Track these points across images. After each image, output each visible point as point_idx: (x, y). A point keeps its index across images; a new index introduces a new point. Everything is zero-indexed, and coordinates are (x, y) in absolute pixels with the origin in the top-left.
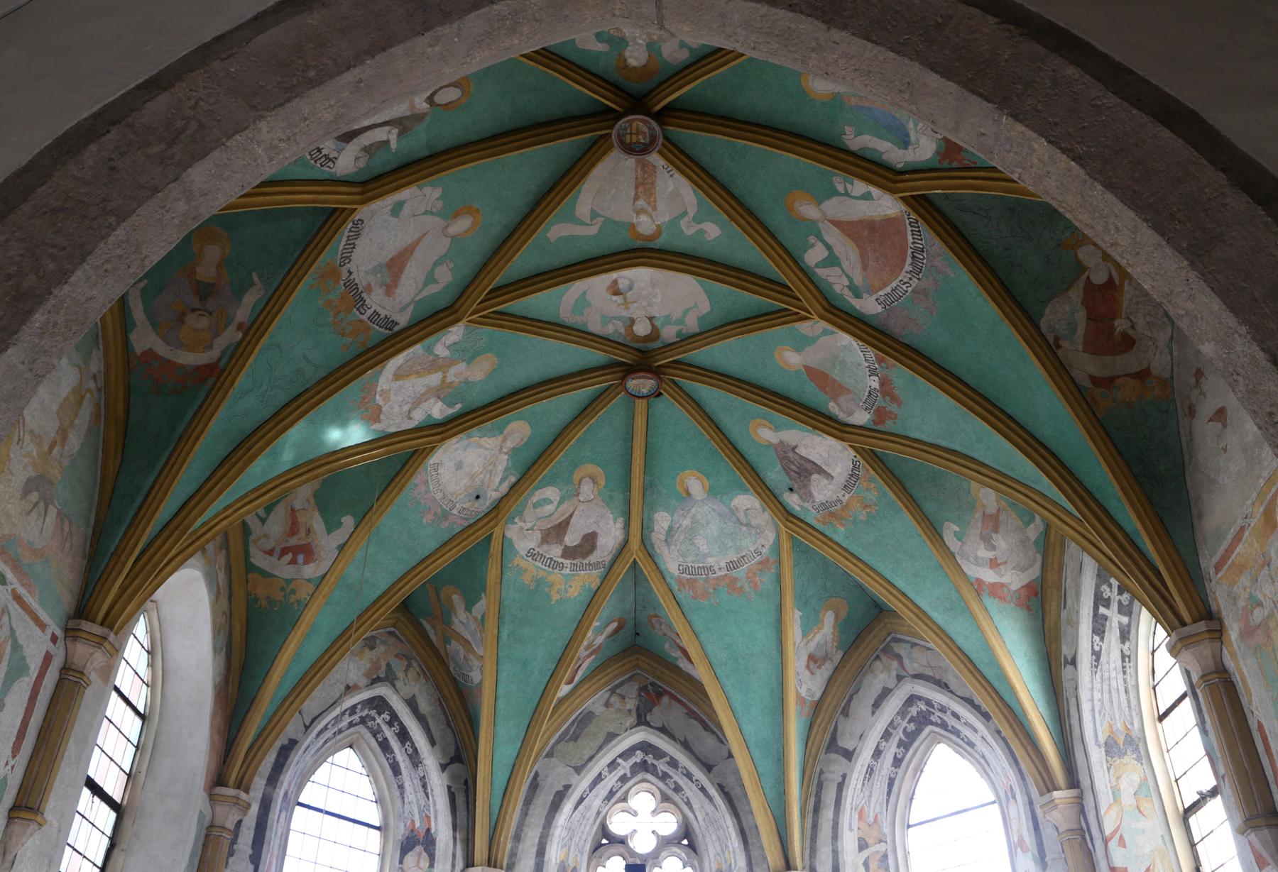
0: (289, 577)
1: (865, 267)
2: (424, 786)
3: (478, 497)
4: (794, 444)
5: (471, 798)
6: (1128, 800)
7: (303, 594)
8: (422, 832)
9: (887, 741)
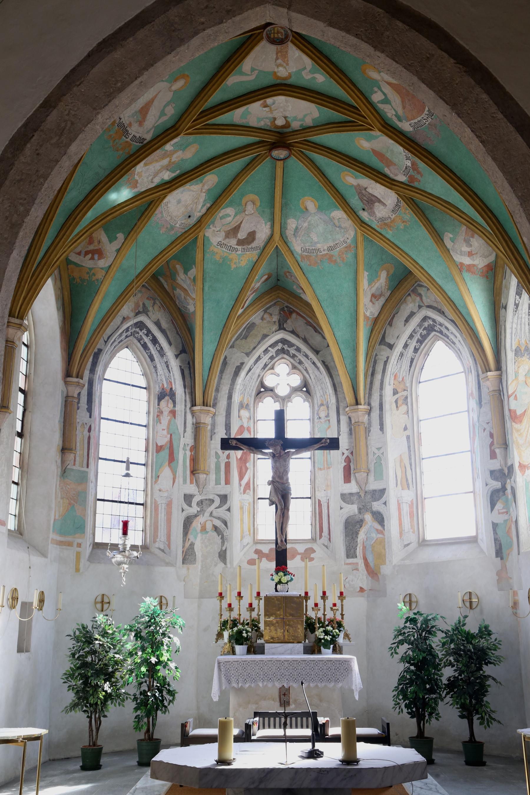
0: (91, 267)
1: (404, 108)
2: (168, 366)
3: (189, 217)
4: (365, 186)
5: (192, 371)
6: (521, 378)
7: (100, 275)
8: (168, 390)
9: (411, 339)
